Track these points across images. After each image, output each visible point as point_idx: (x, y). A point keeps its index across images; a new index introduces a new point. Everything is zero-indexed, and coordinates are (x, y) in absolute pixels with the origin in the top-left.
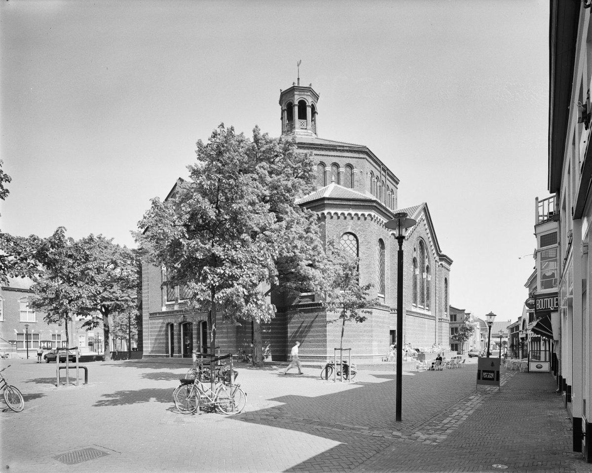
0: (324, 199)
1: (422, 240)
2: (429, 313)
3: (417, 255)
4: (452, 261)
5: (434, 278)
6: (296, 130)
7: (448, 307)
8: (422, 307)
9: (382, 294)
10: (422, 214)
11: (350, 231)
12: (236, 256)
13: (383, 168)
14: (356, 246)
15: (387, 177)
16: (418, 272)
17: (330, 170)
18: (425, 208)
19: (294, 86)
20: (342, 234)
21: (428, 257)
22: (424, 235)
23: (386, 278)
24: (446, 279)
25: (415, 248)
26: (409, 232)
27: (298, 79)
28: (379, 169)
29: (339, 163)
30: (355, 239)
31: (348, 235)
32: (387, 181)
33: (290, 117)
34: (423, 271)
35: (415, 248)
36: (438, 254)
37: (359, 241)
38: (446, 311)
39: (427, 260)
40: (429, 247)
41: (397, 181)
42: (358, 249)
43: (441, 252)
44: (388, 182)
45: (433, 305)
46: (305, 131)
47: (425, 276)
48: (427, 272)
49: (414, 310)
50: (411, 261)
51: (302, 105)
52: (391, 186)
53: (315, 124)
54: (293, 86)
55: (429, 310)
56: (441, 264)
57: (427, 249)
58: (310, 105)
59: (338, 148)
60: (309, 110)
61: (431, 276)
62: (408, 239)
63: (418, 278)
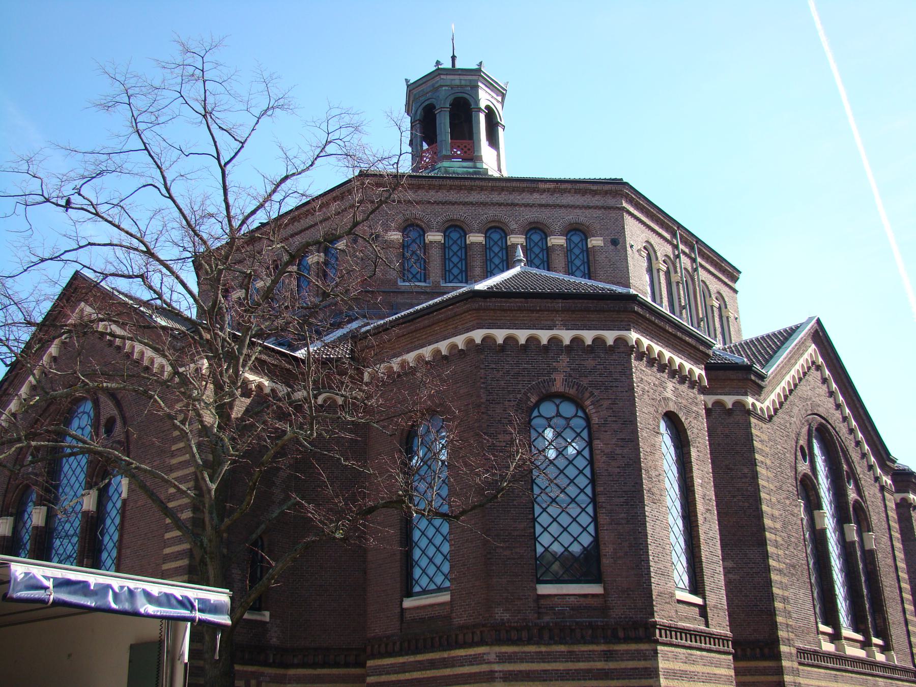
1: (821, 424)
4: (739, 272)
5: (885, 539)
8: (860, 637)
11: (561, 390)
18: (816, 331)
20: (534, 399)
21: (853, 475)
22: (826, 406)
23: (702, 537)
26: (773, 396)
30: (580, 413)
35: (802, 448)
36: (883, 466)
37: (595, 420)
39: (851, 487)
40: (850, 445)
41: (730, 273)
44: (703, 275)
45: (897, 632)
50: (790, 486)
52: (714, 286)
54: (435, 68)
57: (845, 453)
59: (541, 186)
62: (771, 417)
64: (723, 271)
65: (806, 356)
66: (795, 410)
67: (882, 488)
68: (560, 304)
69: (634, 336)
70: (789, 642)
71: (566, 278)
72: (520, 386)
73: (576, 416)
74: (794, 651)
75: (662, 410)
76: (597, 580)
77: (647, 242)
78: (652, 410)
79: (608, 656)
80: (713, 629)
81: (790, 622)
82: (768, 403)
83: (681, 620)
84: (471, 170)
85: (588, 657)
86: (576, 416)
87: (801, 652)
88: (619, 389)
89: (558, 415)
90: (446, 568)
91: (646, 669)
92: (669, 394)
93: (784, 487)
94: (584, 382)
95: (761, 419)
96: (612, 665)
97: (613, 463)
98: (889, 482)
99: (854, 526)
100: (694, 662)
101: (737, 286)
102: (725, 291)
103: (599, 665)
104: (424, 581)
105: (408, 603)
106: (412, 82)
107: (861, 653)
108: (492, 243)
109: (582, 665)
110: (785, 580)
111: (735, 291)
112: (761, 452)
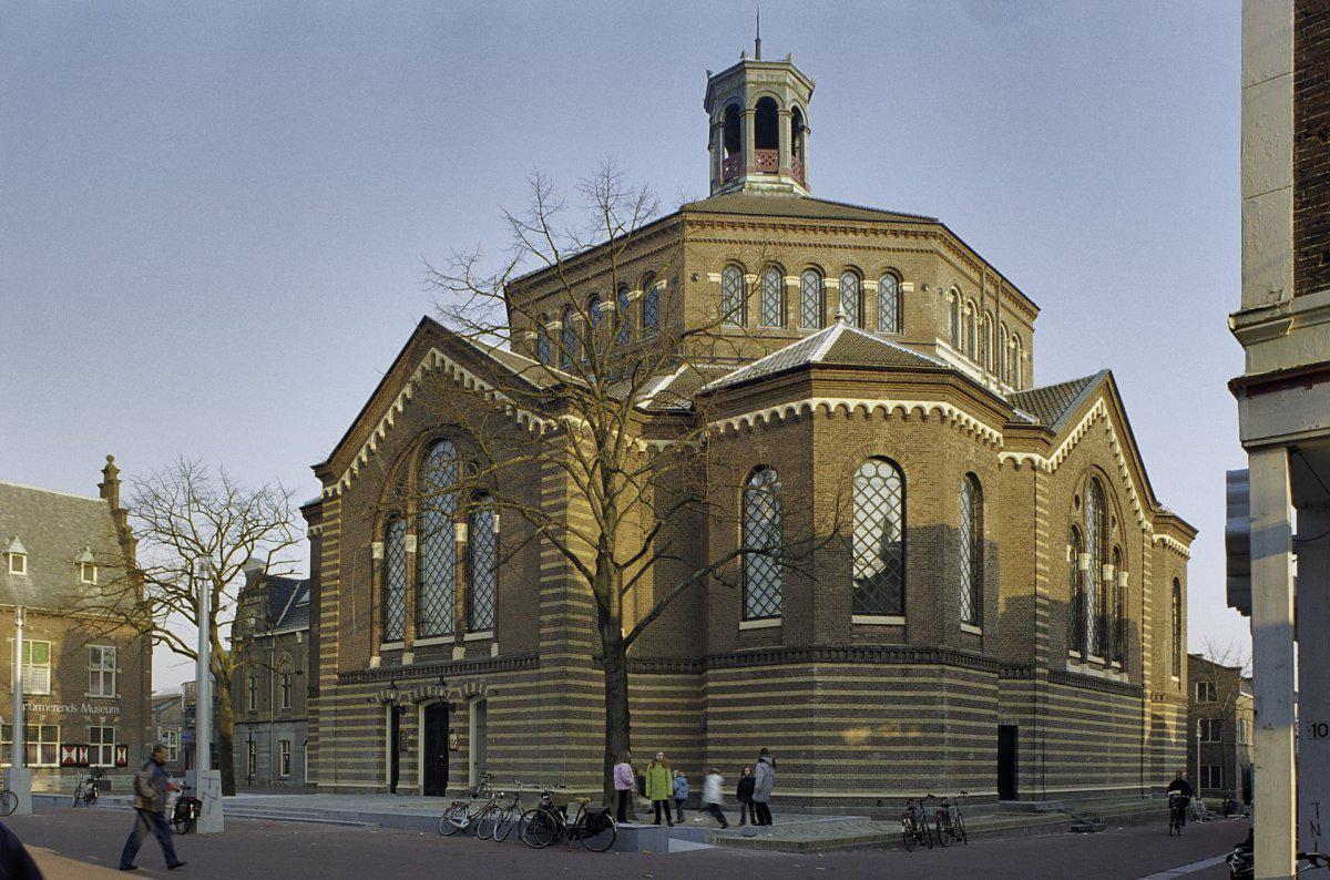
0: (808, 366)
2: (1125, 678)
4: (1196, 532)
5: (1137, 578)
6: (750, 178)
7: (1184, 662)
8: (1101, 661)
9: (974, 624)
10: (1098, 404)
11: (882, 454)
12: (774, 568)
14: (899, 493)
15: (1002, 298)
16: (1086, 562)
17: (837, 285)
19: (743, 62)
23: (986, 579)
24: (1176, 582)
25: (1077, 497)
26: (1059, 452)
27: (758, 41)
28: (975, 276)
30: (896, 474)
31: (877, 462)
33: (734, 142)
34: (1105, 561)
35: (1077, 497)
36: (1148, 509)
37: (908, 481)
38: (1177, 674)
40: (1121, 492)
42: (903, 501)
43: (1160, 505)
44: (1003, 315)
46: (774, 178)
47: (1109, 576)
48: (1117, 563)
49: (1072, 668)
50: (1063, 532)
51: (767, 110)
52: (1013, 325)
53: (802, 158)
54: (740, 61)
55: (1121, 671)
58: (789, 108)
60: (786, 125)
61: (1126, 574)
64: (1024, 309)
65: (1093, 410)
66: (1076, 463)
68: (885, 376)
69: (946, 406)
70: (1043, 665)
72: (847, 450)
73: (892, 476)
74: (1047, 672)
76: (902, 613)
77: (955, 285)
78: (956, 472)
79: (905, 673)
80: (986, 655)
81: (1047, 649)
82: (1053, 458)
83: (963, 647)
84: (775, 186)
86: (892, 476)
88: (931, 454)
89: (877, 475)
90: (778, 599)
93: (1057, 535)
94: (902, 447)
96: (907, 680)
97: (921, 519)
98: (1150, 525)
99: (1111, 567)
100: (969, 680)
101: (1035, 324)
102: (1022, 330)
103: (899, 679)
104: (758, 609)
105: (744, 625)
107: (1100, 674)
108: (807, 286)
109: (885, 679)
110: (1047, 614)
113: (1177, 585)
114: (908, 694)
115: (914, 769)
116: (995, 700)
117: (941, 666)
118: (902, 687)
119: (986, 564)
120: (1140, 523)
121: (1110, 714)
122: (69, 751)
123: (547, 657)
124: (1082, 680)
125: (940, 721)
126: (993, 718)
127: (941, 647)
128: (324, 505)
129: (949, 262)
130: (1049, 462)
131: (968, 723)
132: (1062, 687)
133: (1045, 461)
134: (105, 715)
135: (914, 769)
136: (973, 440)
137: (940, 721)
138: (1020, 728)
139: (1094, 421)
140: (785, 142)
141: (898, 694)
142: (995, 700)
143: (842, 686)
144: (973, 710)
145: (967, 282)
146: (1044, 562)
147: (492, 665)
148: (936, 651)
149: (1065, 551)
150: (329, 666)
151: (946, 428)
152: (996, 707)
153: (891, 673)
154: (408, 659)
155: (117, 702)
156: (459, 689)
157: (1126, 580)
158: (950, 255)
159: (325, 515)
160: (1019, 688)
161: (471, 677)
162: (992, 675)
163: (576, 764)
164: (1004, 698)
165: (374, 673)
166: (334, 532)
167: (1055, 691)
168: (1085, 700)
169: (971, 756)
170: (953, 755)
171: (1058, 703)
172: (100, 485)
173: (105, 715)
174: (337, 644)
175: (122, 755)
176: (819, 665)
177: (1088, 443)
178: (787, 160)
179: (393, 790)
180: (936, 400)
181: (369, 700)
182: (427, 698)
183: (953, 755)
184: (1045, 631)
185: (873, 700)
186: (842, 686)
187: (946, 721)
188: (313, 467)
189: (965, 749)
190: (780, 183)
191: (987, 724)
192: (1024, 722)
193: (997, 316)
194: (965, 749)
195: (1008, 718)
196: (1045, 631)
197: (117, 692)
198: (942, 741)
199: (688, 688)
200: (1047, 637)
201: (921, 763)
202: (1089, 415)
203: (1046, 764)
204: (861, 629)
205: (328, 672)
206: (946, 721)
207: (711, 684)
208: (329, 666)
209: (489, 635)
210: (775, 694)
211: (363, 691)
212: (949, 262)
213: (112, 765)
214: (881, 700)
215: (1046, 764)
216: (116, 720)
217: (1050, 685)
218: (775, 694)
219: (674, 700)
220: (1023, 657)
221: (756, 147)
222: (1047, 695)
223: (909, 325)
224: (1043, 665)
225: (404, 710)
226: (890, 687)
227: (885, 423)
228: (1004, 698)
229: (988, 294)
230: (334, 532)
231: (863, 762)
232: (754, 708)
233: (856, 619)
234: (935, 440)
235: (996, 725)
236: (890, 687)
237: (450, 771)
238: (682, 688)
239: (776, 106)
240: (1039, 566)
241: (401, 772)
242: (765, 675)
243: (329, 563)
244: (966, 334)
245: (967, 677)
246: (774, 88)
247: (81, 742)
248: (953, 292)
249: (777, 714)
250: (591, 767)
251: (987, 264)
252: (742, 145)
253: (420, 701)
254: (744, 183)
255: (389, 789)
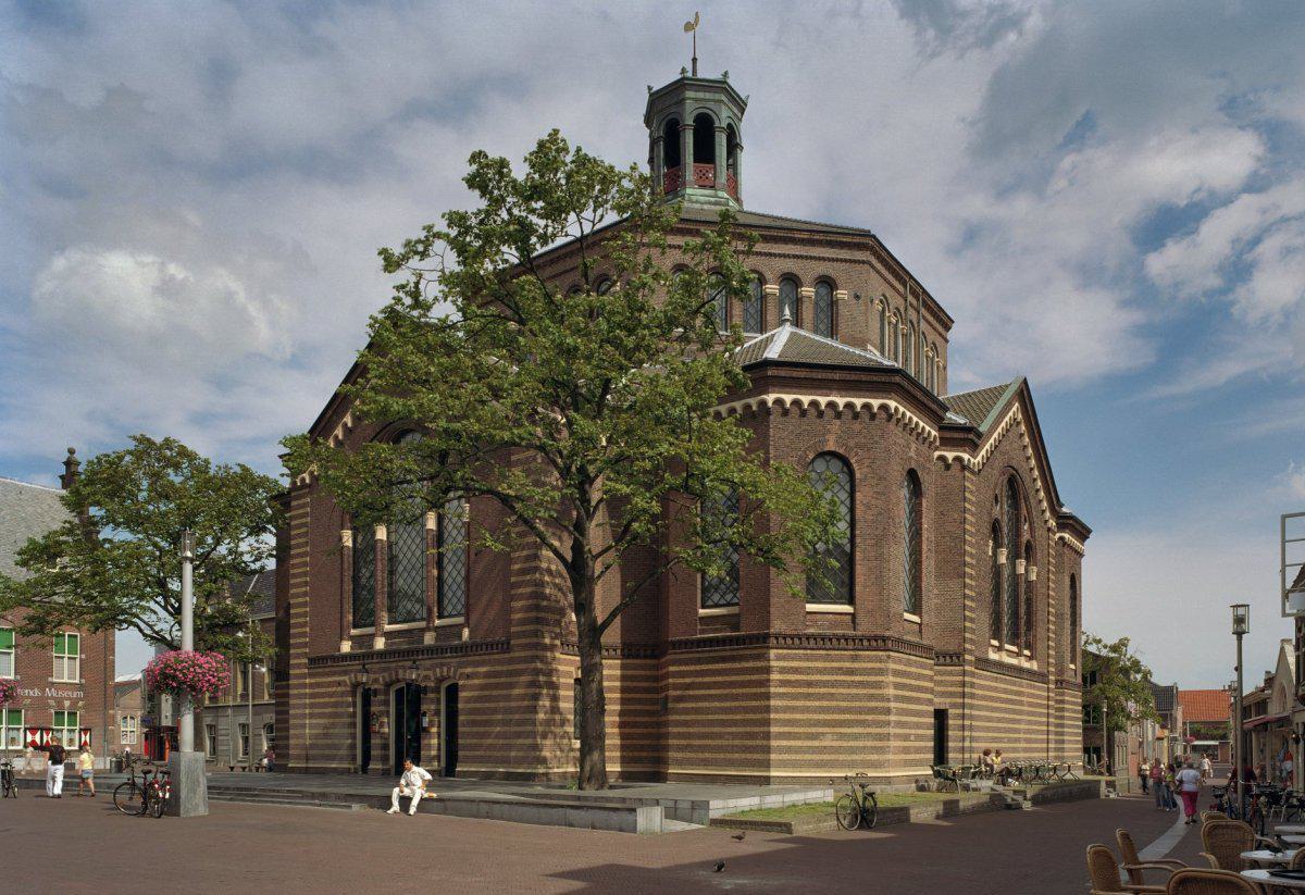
2: (1034, 665)
3: (1001, 511)
4: (1089, 531)
6: (689, 191)
8: (1014, 649)
10: (1014, 409)
11: (833, 449)
13: (924, 301)
14: (847, 487)
15: (923, 310)
20: (811, 456)
23: (924, 571)
25: (996, 496)
26: (983, 452)
27: (694, 60)
29: (800, 273)
32: (922, 322)
35: (996, 496)
37: (858, 475)
40: (1028, 482)
43: (1061, 506)
44: (923, 325)
47: (1021, 570)
48: (1027, 559)
49: (993, 656)
50: (986, 529)
51: (705, 126)
52: (932, 336)
54: (680, 77)
55: (1030, 658)
56: (1061, 538)
57: (1026, 499)
58: (724, 125)
60: (721, 141)
63: (1006, 573)
65: (1011, 414)
67: (1049, 530)
69: (892, 404)
70: (971, 652)
71: (813, 336)
74: (973, 659)
75: (907, 468)
76: (851, 602)
77: (884, 295)
79: (854, 659)
80: (925, 642)
81: (974, 637)
82: (979, 458)
85: (840, 659)
87: (978, 660)
91: (880, 669)
92: (912, 454)
94: (852, 443)
95: (973, 472)
96: (856, 665)
102: (939, 341)
103: (848, 665)
106: (654, 89)
107: (1014, 661)
111: (947, 341)
112: (970, 501)
113: (1074, 582)
114: (857, 678)
115: (863, 749)
116: (931, 685)
117: (887, 653)
118: (851, 672)
119: (924, 556)
120: (1046, 521)
121: (1022, 699)
122: (34, 734)
123: (519, 641)
124: (1000, 665)
125: (885, 704)
126: (930, 702)
127: (887, 634)
128: (293, 494)
129: (878, 272)
130: (976, 461)
131: (808, 703)
132: (985, 673)
133: (972, 460)
134: (69, 699)
135: (863, 749)
136: (913, 438)
137: (885, 704)
138: (950, 711)
139: (1011, 425)
140: (721, 157)
141: (848, 678)
142: (931, 685)
143: (796, 671)
144: (914, 694)
145: (893, 292)
146: (971, 555)
147: (463, 649)
148: (884, 639)
149: (988, 546)
150: (299, 651)
151: (892, 426)
152: (931, 691)
153: (842, 659)
154: (380, 644)
155: (80, 687)
156: (430, 673)
157: (1035, 574)
158: (879, 266)
159: (294, 503)
160: (951, 675)
161: (443, 661)
162: (928, 661)
163: (633, 739)
164: (938, 683)
165: (345, 657)
166: (304, 520)
167: (980, 677)
168: (1002, 686)
169: (912, 738)
170: (897, 736)
171: (982, 687)
172: (61, 477)
173: (69, 699)
174: (308, 629)
175: (86, 738)
176: (776, 651)
177: (1005, 446)
178: (723, 179)
179: (364, 768)
180: (883, 398)
181: (339, 684)
182: (398, 681)
183: (897, 736)
184: (972, 620)
185: (825, 684)
186: (796, 671)
187: (892, 705)
188: (281, 457)
189: (907, 731)
190: (716, 196)
191: (924, 708)
192: (954, 706)
193: (919, 326)
194: (907, 731)
195: (941, 703)
196: (972, 620)
197: (81, 677)
198: (889, 723)
199: (648, 673)
200: (974, 626)
201: (870, 744)
202: (1007, 419)
203: (974, 745)
204: (813, 616)
205: (298, 656)
206: (892, 705)
207: (672, 669)
208: (299, 651)
209: (460, 620)
210: (734, 678)
211: (334, 674)
212: (878, 272)
213: (77, 748)
214: (833, 684)
215: (974, 745)
216: (80, 704)
217: (977, 671)
218: (734, 678)
219: (635, 684)
220: (952, 648)
221: (695, 161)
222: (974, 680)
223: (843, 328)
224: (971, 652)
225: (376, 692)
226: (840, 671)
227: (838, 422)
228: (938, 683)
229: (911, 305)
230: (304, 520)
231: (816, 743)
232: (713, 692)
233: (810, 607)
234: (882, 437)
235: (931, 709)
236: (840, 671)
237: (422, 753)
238: (643, 673)
239: (712, 122)
240: (968, 559)
241: (373, 753)
242: (724, 660)
243: (298, 551)
244: (892, 342)
245: (909, 663)
246: (711, 105)
247: (44, 725)
248: (881, 301)
249: (735, 698)
250: (919, 738)
251: (911, 277)
252: (682, 158)
253: (391, 684)
254: (683, 195)
255: (393, 771)
